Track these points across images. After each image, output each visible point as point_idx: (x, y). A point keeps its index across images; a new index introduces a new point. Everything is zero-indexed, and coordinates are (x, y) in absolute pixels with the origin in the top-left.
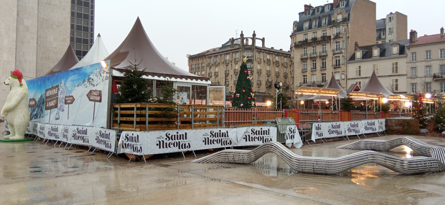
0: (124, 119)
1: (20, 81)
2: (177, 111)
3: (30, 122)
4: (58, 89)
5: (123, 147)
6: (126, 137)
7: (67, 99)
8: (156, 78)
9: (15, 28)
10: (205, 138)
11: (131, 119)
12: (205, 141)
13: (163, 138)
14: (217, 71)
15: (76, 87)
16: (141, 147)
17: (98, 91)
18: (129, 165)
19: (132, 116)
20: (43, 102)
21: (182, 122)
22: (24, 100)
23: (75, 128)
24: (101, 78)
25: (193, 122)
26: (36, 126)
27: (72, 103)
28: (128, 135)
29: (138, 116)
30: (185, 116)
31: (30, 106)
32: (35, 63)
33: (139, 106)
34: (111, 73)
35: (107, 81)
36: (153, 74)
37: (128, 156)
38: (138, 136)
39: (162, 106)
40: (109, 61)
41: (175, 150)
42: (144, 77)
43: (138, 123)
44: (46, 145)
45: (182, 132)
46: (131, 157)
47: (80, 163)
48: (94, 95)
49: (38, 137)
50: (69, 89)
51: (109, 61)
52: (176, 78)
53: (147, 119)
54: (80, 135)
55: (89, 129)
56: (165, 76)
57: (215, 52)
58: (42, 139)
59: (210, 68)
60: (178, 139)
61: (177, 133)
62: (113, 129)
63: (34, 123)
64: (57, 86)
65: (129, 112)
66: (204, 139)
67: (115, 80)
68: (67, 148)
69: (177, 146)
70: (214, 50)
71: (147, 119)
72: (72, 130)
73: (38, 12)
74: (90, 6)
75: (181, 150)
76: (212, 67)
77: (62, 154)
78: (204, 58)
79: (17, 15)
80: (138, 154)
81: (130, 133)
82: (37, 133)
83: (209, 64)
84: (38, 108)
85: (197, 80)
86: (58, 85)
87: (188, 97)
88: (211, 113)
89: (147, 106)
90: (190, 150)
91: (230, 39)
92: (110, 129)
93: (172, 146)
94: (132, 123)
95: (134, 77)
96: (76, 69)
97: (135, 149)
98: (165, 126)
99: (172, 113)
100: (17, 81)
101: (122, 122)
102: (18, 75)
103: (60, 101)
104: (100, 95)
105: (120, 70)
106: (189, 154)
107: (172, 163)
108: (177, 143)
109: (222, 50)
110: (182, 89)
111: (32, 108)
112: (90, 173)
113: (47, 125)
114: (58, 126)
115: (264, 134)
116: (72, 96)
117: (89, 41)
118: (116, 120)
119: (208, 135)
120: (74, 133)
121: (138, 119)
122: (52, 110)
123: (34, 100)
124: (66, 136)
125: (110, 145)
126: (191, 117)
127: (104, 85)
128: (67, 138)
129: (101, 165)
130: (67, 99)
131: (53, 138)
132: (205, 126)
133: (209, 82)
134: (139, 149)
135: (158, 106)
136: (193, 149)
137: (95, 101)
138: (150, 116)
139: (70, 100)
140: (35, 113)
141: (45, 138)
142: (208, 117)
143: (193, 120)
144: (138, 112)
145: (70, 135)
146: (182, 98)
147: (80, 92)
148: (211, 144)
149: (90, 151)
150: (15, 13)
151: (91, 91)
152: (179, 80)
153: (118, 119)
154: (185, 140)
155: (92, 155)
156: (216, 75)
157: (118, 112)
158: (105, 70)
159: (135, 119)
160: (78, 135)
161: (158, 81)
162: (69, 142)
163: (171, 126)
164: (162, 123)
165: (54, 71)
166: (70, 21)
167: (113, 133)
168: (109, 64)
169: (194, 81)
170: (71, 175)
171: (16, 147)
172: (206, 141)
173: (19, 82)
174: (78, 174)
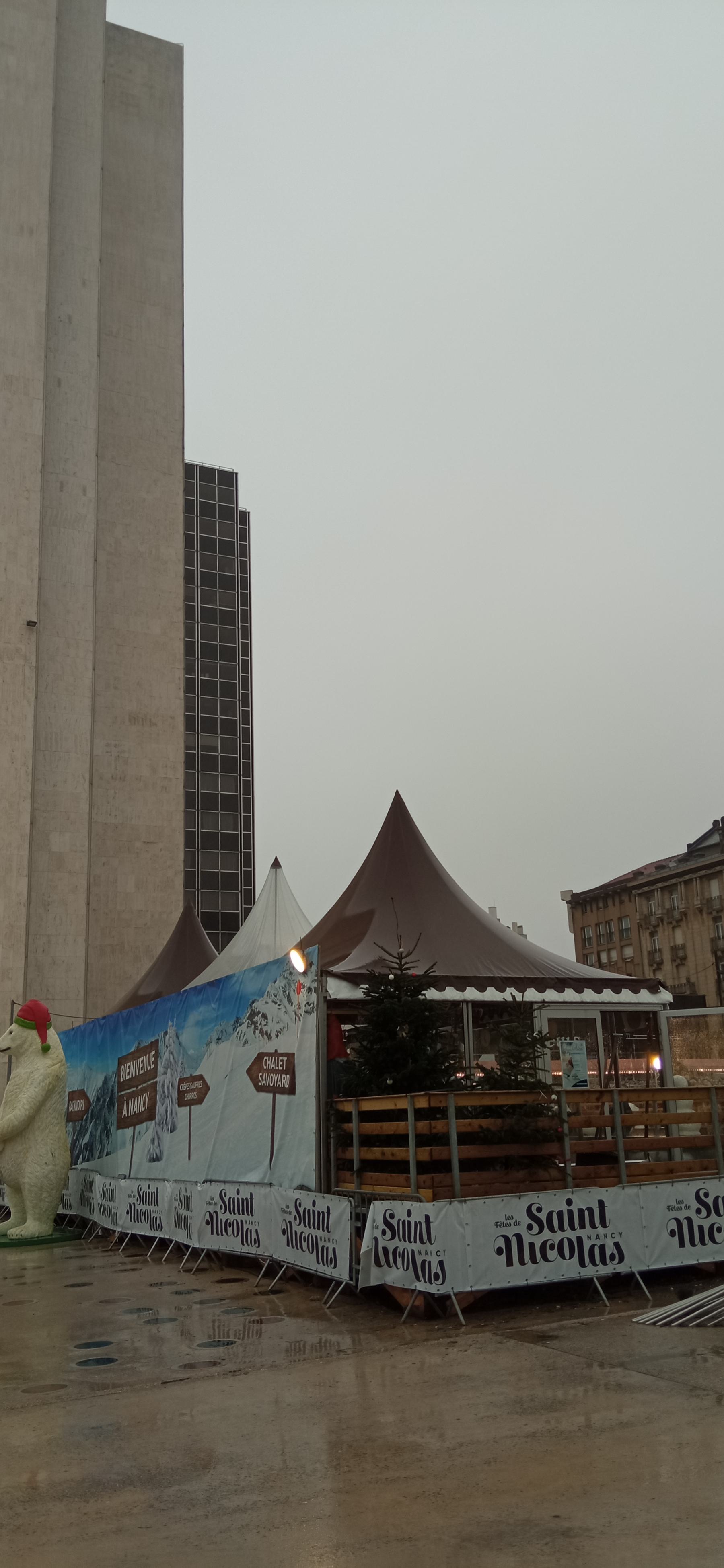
0: (375, 1153)
1: (43, 1037)
2: (558, 1115)
3: (71, 1174)
4: (157, 1056)
5: (378, 1264)
6: (386, 1222)
7: (185, 1086)
8: (471, 994)
9: (26, 863)
10: (677, 1220)
11: (398, 1153)
12: (677, 1233)
13: (517, 1224)
14: (679, 941)
15: (213, 1046)
16: (441, 1263)
17: (282, 1055)
18: (407, 1332)
19: (401, 1140)
20: (111, 1103)
21: (583, 1159)
22: (55, 1097)
23: (214, 1190)
24: (291, 1009)
25: (622, 1154)
26: (88, 1185)
27: (200, 1101)
28: (392, 1216)
29: (423, 1140)
30: (591, 1131)
31: (70, 1117)
32: (83, 966)
33: (422, 1103)
34: (321, 989)
35: (312, 1019)
36: (461, 983)
37: (397, 1295)
38: (427, 1218)
39: (502, 1101)
40: (314, 949)
41: (567, 1270)
42: (432, 994)
43: (423, 1167)
44: (120, 1257)
45: (585, 1198)
46: (408, 1302)
47: (236, 1322)
48: (270, 1071)
49: (95, 1223)
50: (191, 1052)
51: (314, 949)
52: (541, 991)
53: (456, 1152)
54: (232, 1217)
55: (259, 1193)
56: (501, 984)
57: (664, 873)
58: (107, 1232)
59: (652, 934)
60: (572, 1227)
61: (569, 1202)
62: (339, 1194)
63: (83, 1174)
64: (154, 1045)
65: (389, 1127)
66: (673, 1225)
67: (335, 1012)
68: (189, 1265)
69: (571, 1256)
70: (660, 866)
71: (456, 1152)
72: (204, 1197)
73: (91, 806)
74: (240, 769)
75: (589, 1271)
76: (660, 929)
77: (174, 1288)
78: (625, 898)
79: (31, 823)
80: (433, 1288)
81: (400, 1209)
82: (91, 1211)
83: (646, 918)
84: (95, 1121)
85: (617, 991)
86: (157, 1041)
87: (592, 1051)
88: (688, 1119)
89: (452, 1103)
90: (623, 1269)
91: (716, 823)
92: (329, 1192)
93: (552, 1254)
94: (401, 1167)
95: (399, 999)
96: (212, 984)
97: (420, 1270)
98: (521, 1174)
99: (540, 1124)
100: (33, 1035)
101: (368, 1165)
102: (35, 1018)
103: (164, 1098)
104: (290, 1069)
105: (352, 979)
106: (621, 1287)
107: (562, 1328)
108: (570, 1241)
109: (692, 865)
110: (565, 1028)
111: (78, 1124)
112: (274, 1367)
113: (123, 1182)
114: (160, 1185)
115: (582, 1226)
116: (201, 1077)
117: (241, 879)
118: (349, 1159)
119: (688, 1208)
120: (211, 1209)
121: (424, 1154)
122: (137, 1127)
123: (80, 1094)
124: (185, 1219)
125: (331, 1255)
126: (609, 1137)
127: (303, 1031)
128: (188, 1228)
129: (308, 1331)
130: (185, 1086)
131: (142, 1229)
132: (671, 1171)
133: (666, 996)
134: (435, 1268)
135: (487, 1102)
136: (633, 1265)
137: (275, 1090)
138: (464, 1139)
139: (194, 1091)
140: (86, 1139)
141: (118, 1229)
142: (675, 1134)
143: (621, 1146)
144: (423, 1126)
145: (198, 1215)
146: (570, 1063)
147: (224, 1062)
148: (703, 1242)
149: (266, 1275)
150: (26, 819)
151: (260, 1057)
152: (550, 995)
153: (355, 1153)
154: (600, 1230)
155: (274, 1292)
156: (679, 957)
157: (353, 1126)
158: (302, 980)
159: (411, 1153)
160: (223, 1217)
161: (476, 1004)
162: (195, 1244)
163: (542, 1174)
164: (507, 1163)
165: (141, 992)
166: (182, 824)
167: (340, 1209)
168: (315, 959)
169: (607, 995)
170: (212, 1377)
171: (29, 1265)
172: (684, 1232)
173: (38, 1040)
174: (235, 1373)
